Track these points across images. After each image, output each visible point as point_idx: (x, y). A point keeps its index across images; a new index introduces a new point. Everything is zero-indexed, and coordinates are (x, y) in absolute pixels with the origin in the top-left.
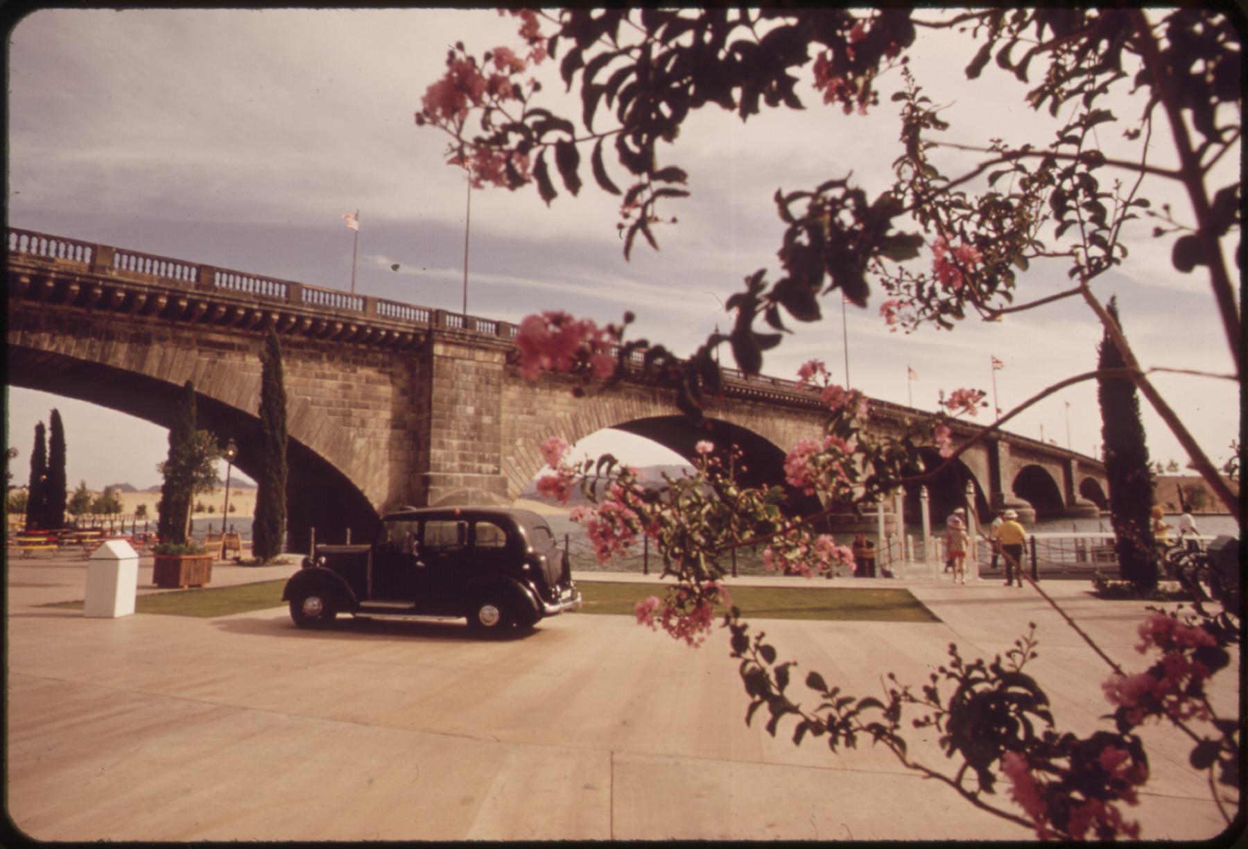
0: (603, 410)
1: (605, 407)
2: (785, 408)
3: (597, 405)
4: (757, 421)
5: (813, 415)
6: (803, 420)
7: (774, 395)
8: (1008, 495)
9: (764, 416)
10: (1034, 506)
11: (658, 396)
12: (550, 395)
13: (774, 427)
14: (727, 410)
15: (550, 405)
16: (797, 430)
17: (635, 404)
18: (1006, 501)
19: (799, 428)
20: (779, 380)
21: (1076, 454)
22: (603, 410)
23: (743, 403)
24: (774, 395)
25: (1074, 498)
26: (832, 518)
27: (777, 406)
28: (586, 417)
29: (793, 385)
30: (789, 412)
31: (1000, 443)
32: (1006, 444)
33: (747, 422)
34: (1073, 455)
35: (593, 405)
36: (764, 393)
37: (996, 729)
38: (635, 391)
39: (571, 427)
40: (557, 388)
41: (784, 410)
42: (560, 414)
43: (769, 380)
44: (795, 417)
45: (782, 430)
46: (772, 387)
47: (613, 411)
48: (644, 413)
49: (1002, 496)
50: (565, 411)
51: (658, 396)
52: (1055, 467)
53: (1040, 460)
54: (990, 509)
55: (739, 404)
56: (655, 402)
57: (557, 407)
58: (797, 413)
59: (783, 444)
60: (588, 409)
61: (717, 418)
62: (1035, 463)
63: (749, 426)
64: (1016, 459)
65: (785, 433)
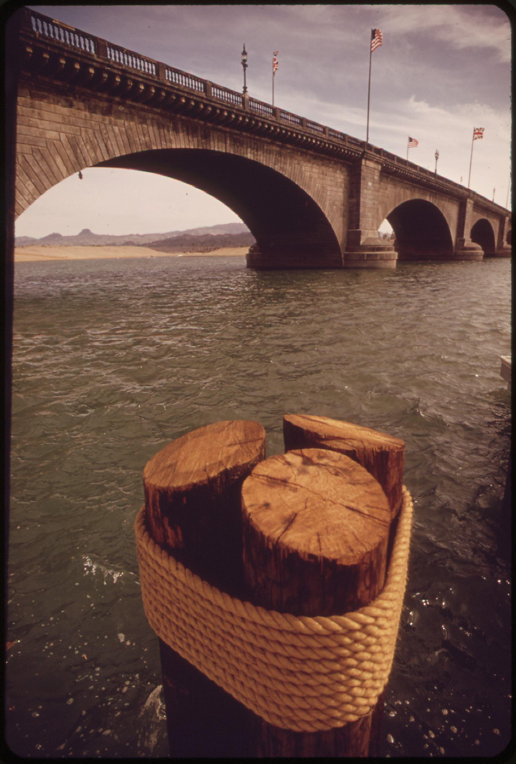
0: (111, 134)
1: (113, 130)
2: (311, 152)
3: (103, 127)
4: (285, 163)
5: (336, 163)
6: (327, 166)
7: (302, 136)
8: (468, 240)
9: (292, 157)
10: (483, 249)
11: (179, 126)
12: (32, 106)
13: (301, 172)
14: (257, 147)
15: (35, 120)
16: (321, 176)
17: (152, 130)
18: (466, 244)
19: (323, 174)
20: (308, 121)
21: (474, 193)
22: (111, 134)
23: (272, 144)
24: (302, 136)
25: (503, 243)
26: (346, 255)
27: (304, 150)
28: (89, 141)
29: (318, 128)
30: (315, 158)
31: (468, 200)
32: (472, 202)
33: (275, 164)
34: (471, 194)
35: (97, 127)
36: (292, 133)
37: (44, 650)
38: (151, 115)
39: (69, 152)
40: (42, 98)
41: (311, 155)
42: (52, 135)
43: (321, 129)
44: (320, 163)
45: (308, 174)
46: (300, 128)
47: (125, 138)
48: (164, 143)
49: (463, 241)
50: (59, 131)
51: (179, 126)
52: (495, 221)
53: (236, 142)
54: (343, 252)
55: (268, 143)
56: (176, 130)
57: (46, 124)
58: (322, 159)
59: (309, 188)
60: (90, 131)
61: (245, 156)
62: (485, 218)
63: (277, 168)
64: (475, 214)
65: (311, 177)
